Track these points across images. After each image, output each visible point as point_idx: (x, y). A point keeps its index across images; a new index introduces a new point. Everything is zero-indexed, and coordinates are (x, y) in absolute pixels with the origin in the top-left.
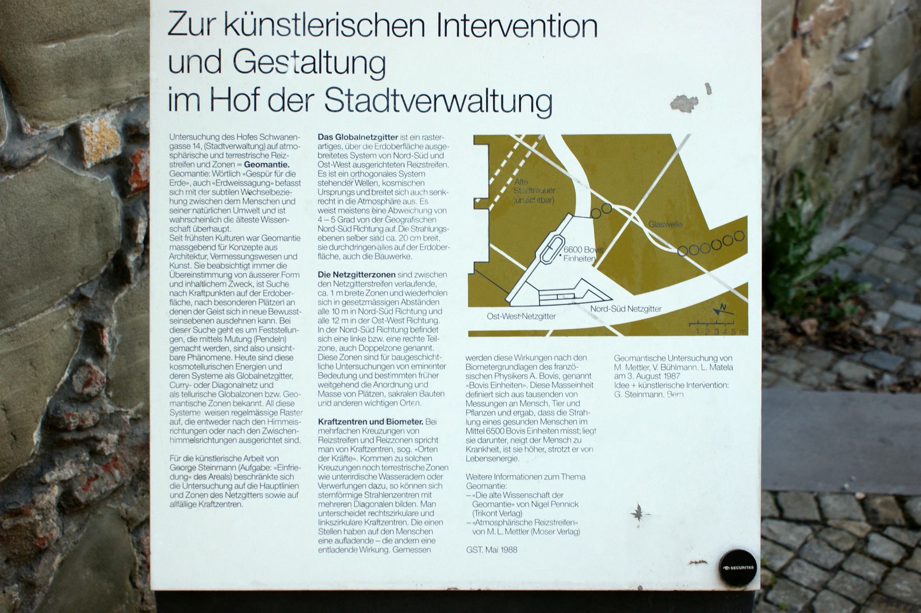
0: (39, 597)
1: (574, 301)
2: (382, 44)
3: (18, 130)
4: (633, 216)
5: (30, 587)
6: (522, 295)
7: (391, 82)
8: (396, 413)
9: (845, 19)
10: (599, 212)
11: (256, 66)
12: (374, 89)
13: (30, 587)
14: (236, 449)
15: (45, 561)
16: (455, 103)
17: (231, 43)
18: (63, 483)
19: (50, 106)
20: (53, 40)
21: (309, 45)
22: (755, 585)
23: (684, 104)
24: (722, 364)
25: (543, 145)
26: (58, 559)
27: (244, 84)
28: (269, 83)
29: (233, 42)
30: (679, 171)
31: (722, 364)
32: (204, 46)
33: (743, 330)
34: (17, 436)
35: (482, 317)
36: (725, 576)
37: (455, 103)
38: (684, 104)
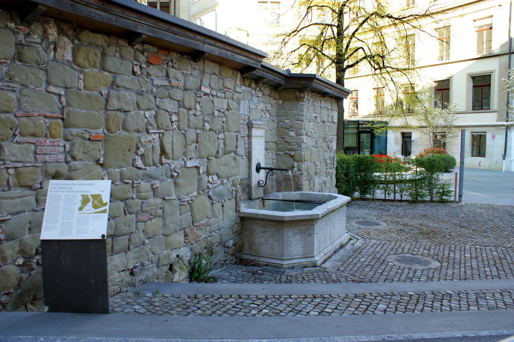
0: (31, 277)
1: (89, 210)
2: (73, 186)
3: (37, 207)
4: (96, 202)
5: (30, 275)
6: (84, 210)
7: (73, 190)
8: (69, 221)
9: (459, 294)
10: (93, 202)
11: (59, 188)
12: (71, 190)
13: (30, 275)
14: (52, 225)
15: (33, 271)
16: (79, 192)
17: (57, 186)
18: (37, 259)
19: (42, 205)
20: (43, 196)
21: (65, 186)
22: (105, 238)
23: (102, 191)
24: (104, 216)
25: (88, 196)
26: (35, 272)
27: (58, 190)
28: (60, 190)
29: (57, 186)
30: (101, 197)
31: (104, 216)
32: (54, 186)
33: (106, 213)
34: (32, 250)
35: (80, 212)
36: (102, 237)
37: (79, 192)
38: (102, 191)
